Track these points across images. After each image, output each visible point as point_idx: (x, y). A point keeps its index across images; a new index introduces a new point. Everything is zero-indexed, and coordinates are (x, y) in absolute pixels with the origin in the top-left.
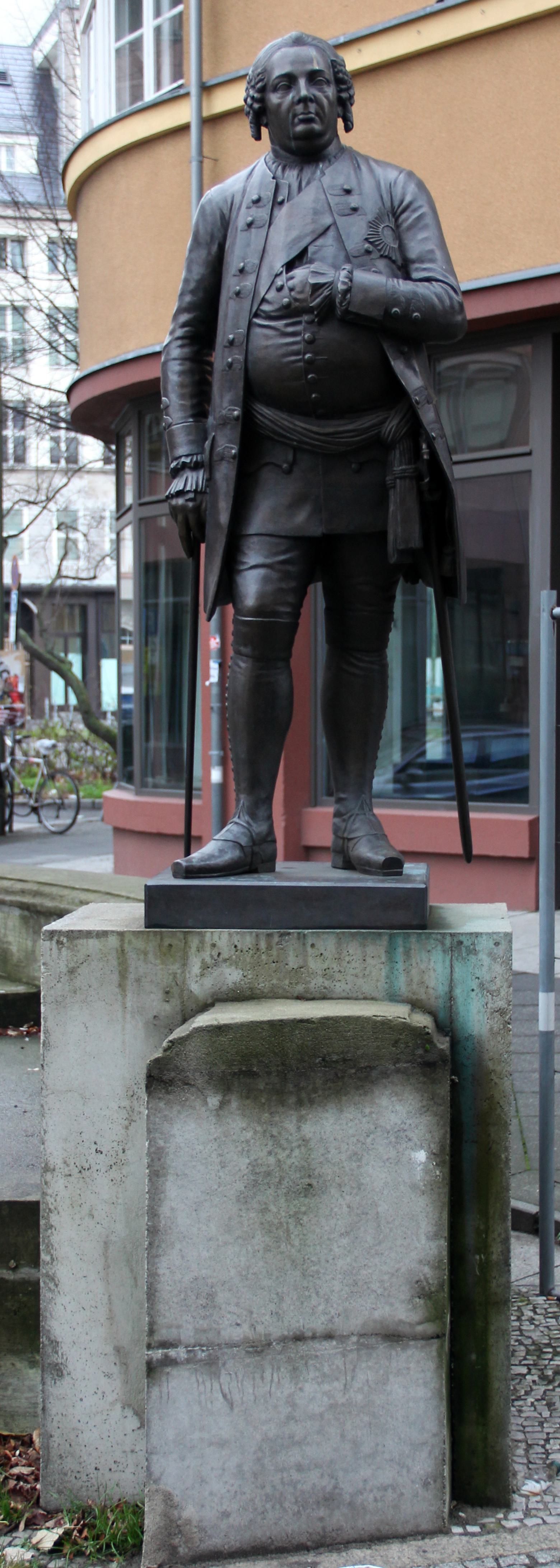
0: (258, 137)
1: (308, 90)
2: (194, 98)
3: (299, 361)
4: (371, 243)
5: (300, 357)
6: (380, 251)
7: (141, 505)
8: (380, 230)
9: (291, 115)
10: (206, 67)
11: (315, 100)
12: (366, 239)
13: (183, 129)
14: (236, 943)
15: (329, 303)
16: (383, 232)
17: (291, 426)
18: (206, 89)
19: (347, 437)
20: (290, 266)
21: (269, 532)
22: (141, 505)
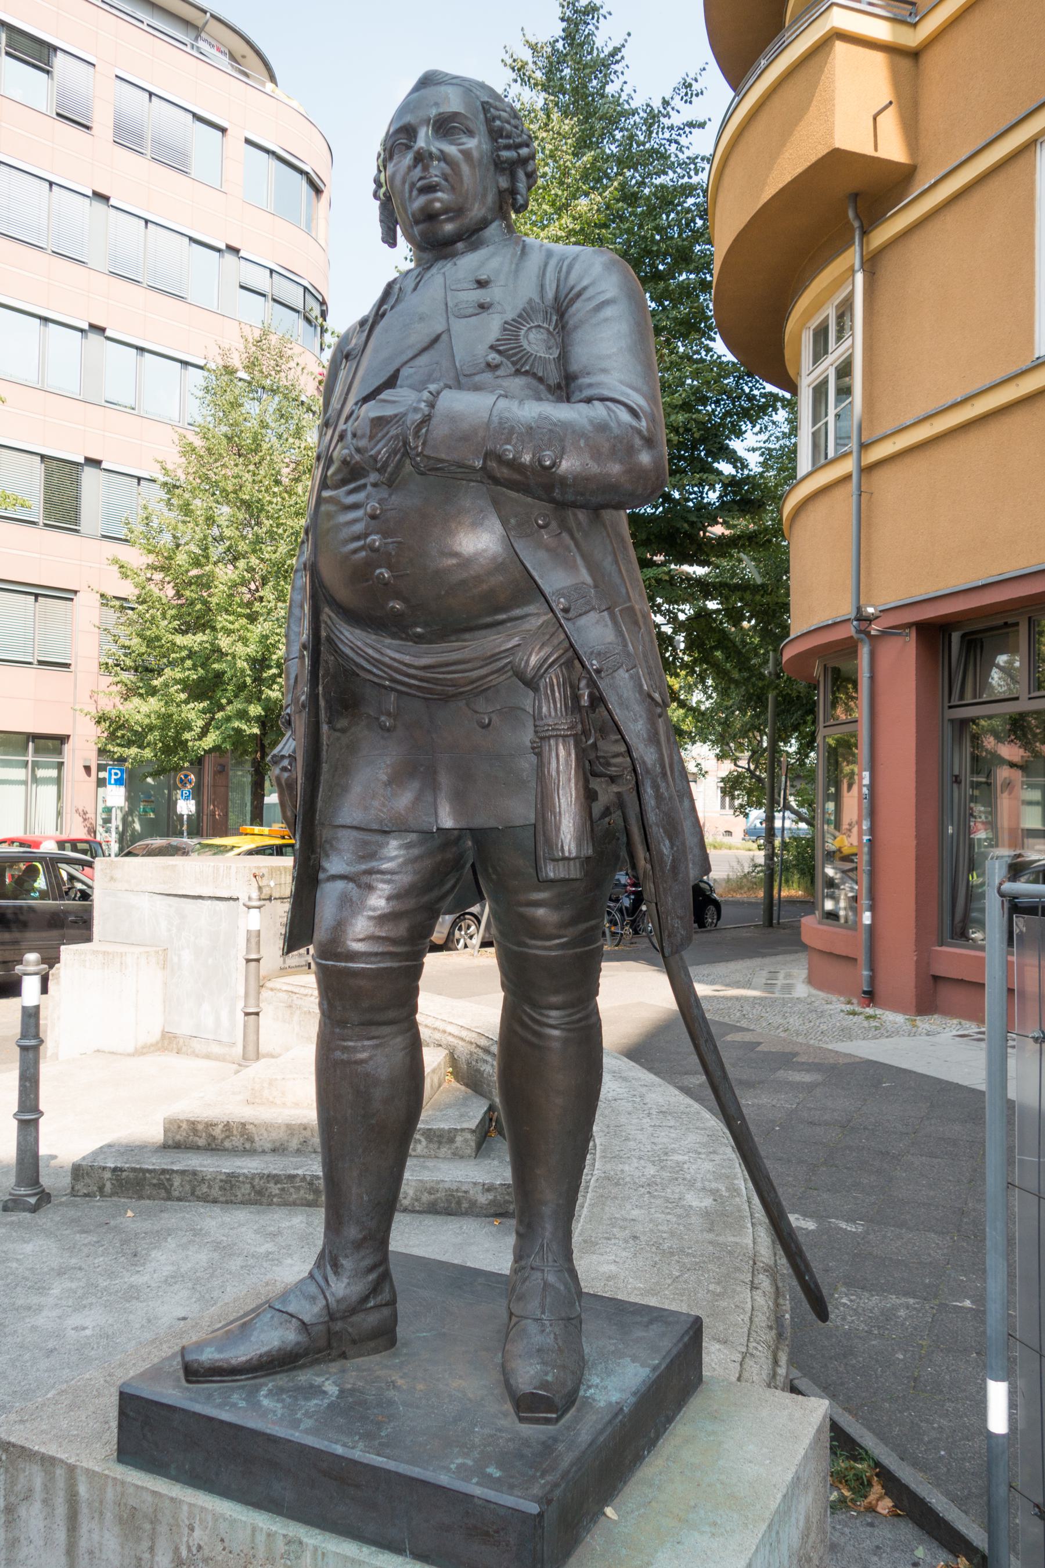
0: (393, 244)
1: (428, 143)
2: (855, 454)
3: (362, 548)
4: (499, 352)
5: (361, 543)
6: (514, 363)
7: (1030, 699)
8: (522, 332)
9: (407, 186)
10: (864, 433)
11: (444, 157)
12: (492, 347)
13: (848, 477)
14: (224, 1536)
15: (404, 450)
16: (526, 336)
17: (377, 656)
18: (863, 447)
19: (443, 673)
20: (366, 399)
21: (355, 823)
22: (1030, 699)
